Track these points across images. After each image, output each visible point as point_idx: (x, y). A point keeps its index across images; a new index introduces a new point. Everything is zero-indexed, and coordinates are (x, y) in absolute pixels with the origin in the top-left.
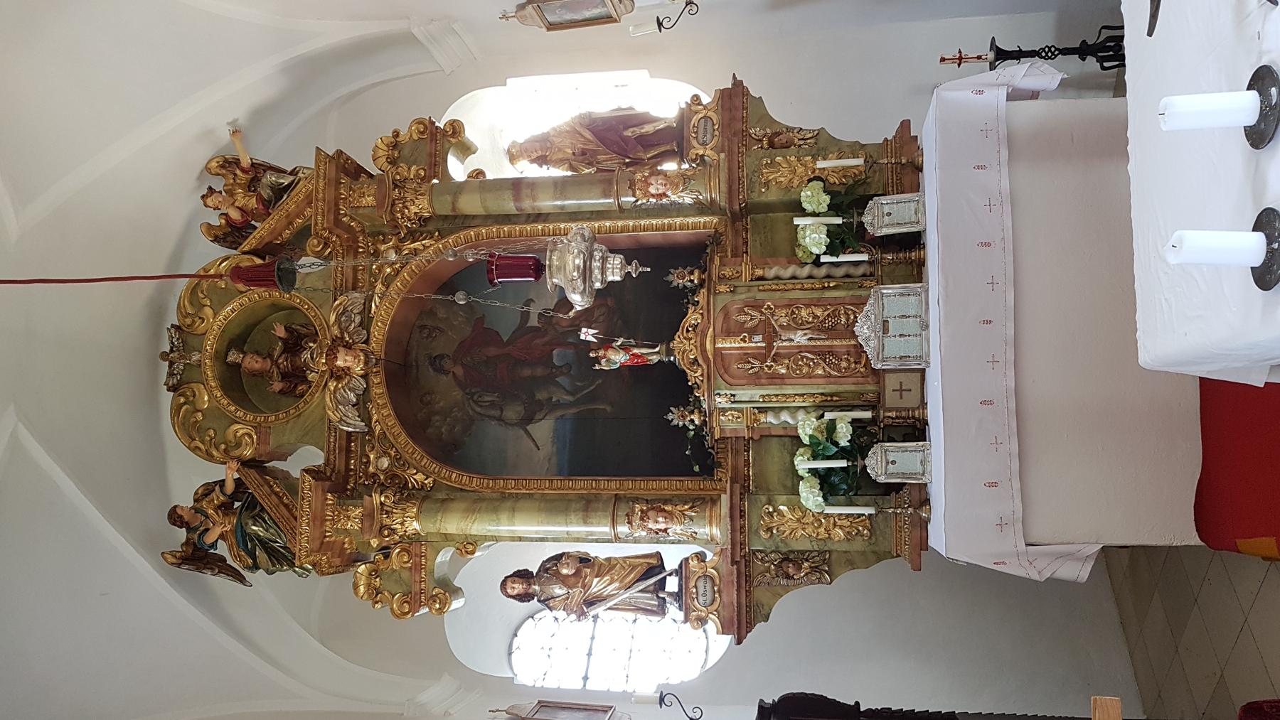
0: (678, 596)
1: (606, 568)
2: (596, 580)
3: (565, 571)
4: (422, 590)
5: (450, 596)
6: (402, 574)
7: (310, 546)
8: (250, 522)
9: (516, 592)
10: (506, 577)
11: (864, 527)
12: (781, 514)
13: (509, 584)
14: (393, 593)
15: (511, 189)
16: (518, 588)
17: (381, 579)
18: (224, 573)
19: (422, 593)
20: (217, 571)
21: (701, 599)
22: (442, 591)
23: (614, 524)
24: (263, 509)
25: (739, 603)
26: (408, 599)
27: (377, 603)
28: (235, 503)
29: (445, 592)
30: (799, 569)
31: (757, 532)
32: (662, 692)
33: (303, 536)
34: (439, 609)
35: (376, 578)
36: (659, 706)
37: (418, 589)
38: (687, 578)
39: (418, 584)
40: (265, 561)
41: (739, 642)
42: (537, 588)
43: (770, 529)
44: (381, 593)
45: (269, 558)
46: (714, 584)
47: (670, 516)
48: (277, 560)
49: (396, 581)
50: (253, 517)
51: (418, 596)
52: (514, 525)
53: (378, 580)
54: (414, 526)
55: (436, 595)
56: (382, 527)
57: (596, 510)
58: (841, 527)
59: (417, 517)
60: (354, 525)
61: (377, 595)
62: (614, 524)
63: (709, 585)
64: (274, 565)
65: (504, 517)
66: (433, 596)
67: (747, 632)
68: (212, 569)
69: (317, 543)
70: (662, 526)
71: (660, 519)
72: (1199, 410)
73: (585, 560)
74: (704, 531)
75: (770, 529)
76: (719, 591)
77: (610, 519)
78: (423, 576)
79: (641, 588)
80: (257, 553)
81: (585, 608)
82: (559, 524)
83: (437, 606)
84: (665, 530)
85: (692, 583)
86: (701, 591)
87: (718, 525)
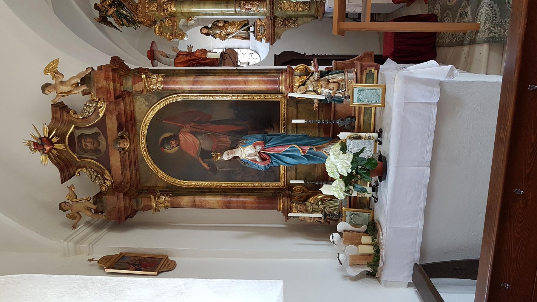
0: (254, 32)
1: (232, 23)
2: (229, 27)
3: (220, 25)
8: (121, 9)
9: (205, 32)
10: (202, 28)
11: (307, 7)
12: (284, 3)
13: (203, 30)
16: (205, 31)
21: (261, 32)
23: (235, 8)
24: (124, 5)
25: (272, 33)
30: (289, 22)
31: (277, 9)
38: (257, 26)
42: (211, 32)
43: (281, 8)
46: (264, 28)
47: (252, 5)
49: (167, 30)
50: (121, 8)
52: (205, 8)
54: (174, 9)
55: (180, 34)
56: (164, 9)
57: (230, 4)
58: (301, 7)
59: (175, 6)
60: (155, 9)
62: (235, 8)
63: (263, 28)
65: (202, 5)
70: (250, 7)
71: (249, 5)
73: (225, 22)
74: (262, 10)
75: (281, 8)
76: (266, 30)
77: (234, 6)
79: (243, 29)
82: (219, 8)
84: (250, 9)
85: (258, 27)
86: (261, 30)
87: (266, 7)
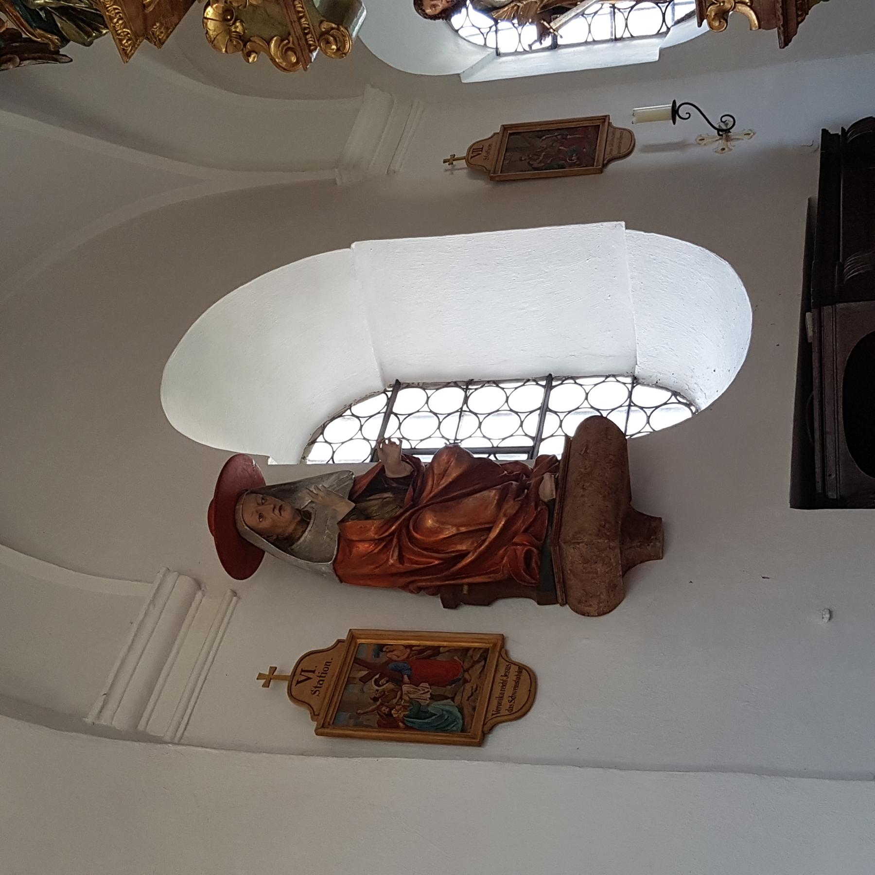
4: (305, 28)
5: (346, 29)
6: (269, 11)
7: (131, 30)
14: (266, 36)
15: (220, 21)
17: (242, 22)
18: (28, 59)
19: (307, 34)
20: (18, 60)
22: (334, 25)
26: (291, 45)
27: (249, 55)
28: (23, 37)
29: (338, 25)
32: (674, 102)
33: (115, 20)
34: (338, 49)
35: (234, 23)
36: (671, 121)
37: (299, 32)
39: (297, 24)
40: (74, 32)
41: (786, 41)
44: (250, 40)
45: (78, 26)
48: (89, 25)
51: (304, 41)
53: (238, 24)
55: (327, 32)
61: (245, 46)
64: (89, 35)
66: (323, 34)
67: (798, 23)
68: (10, 60)
69: (139, 23)
72: (858, 120)
78: (300, 9)
80: (59, 25)
81: (545, 23)
83: (334, 47)
